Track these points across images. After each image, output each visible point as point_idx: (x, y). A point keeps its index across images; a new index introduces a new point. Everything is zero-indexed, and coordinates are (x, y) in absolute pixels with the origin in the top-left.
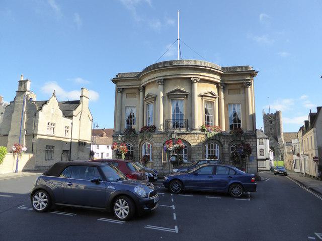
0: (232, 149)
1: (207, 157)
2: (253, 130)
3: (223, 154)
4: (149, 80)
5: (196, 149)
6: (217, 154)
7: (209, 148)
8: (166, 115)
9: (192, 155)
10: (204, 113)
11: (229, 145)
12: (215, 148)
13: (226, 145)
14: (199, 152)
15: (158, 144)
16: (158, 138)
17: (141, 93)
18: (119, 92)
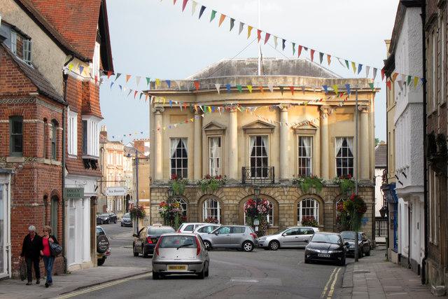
0: (340, 209)
1: (55, 162)
2: (370, 177)
3: (324, 215)
4: (213, 101)
5: (286, 208)
6: (316, 215)
7: (304, 205)
8: (243, 159)
9: (280, 216)
10: (298, 165)
11: (335, 201)
12: (313, 206)
13: (329, 202)
14: (289, 212)
15: (231, 202)
16: (230, 194)
17: (197, 118)
18: (158, 113)
